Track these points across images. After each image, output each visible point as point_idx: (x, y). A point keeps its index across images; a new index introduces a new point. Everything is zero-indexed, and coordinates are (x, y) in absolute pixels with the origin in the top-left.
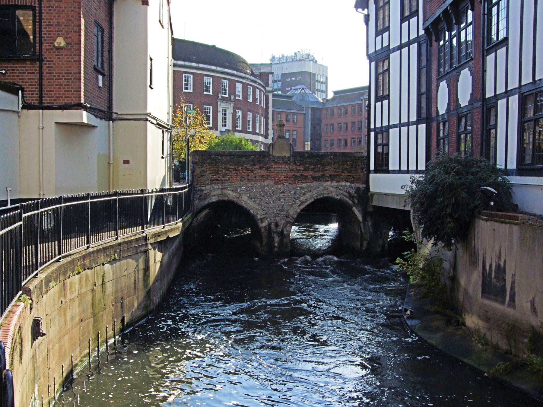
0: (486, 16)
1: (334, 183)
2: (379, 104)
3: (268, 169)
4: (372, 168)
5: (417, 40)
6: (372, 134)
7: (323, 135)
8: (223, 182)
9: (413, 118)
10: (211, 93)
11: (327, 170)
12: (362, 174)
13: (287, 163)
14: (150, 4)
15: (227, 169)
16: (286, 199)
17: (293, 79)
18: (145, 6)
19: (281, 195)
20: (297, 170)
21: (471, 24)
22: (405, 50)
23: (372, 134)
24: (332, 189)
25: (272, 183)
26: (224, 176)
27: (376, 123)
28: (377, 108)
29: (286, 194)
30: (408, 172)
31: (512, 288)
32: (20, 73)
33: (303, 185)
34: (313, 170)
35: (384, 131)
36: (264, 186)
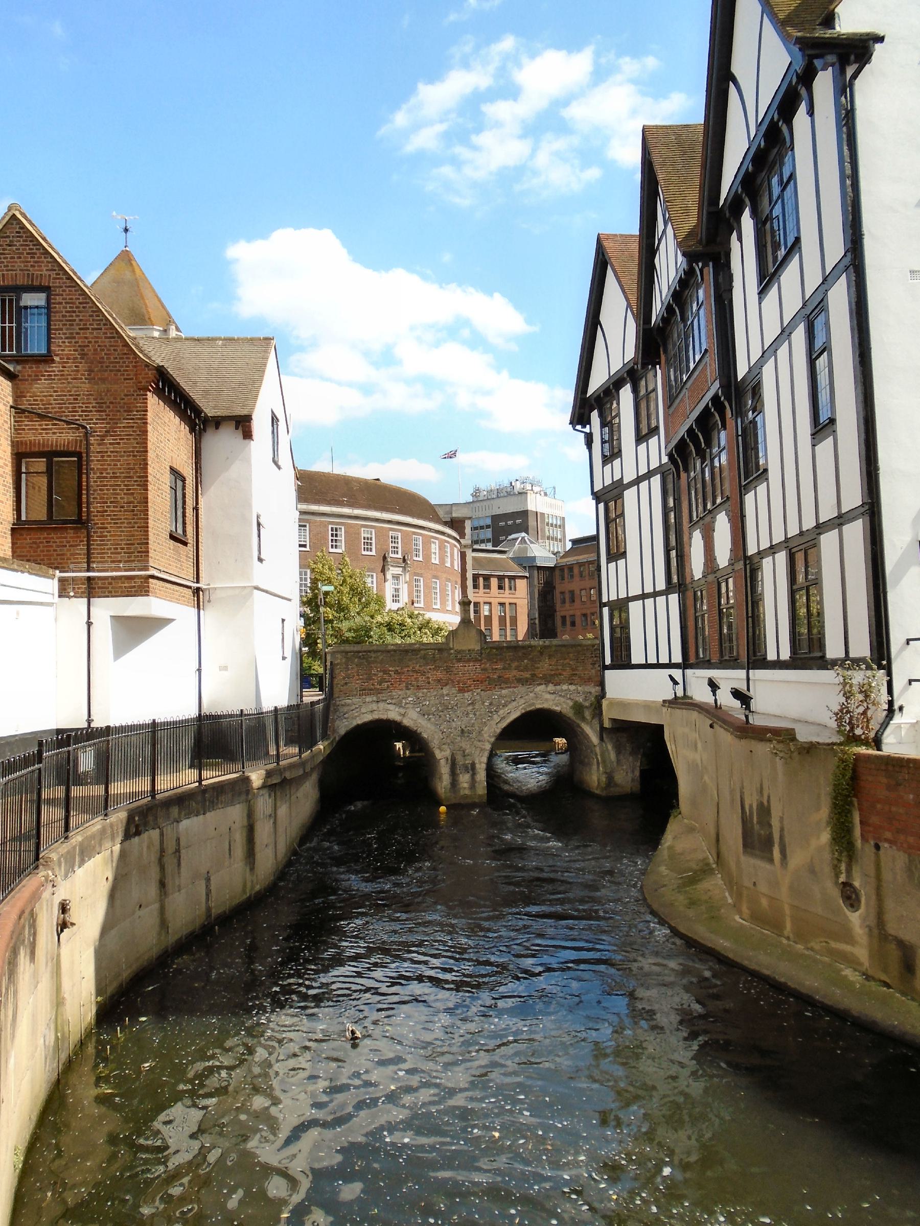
0: (740, 438)
1: (551, 687)
2: (612, 565)
3: (448, 670)
4: (608, 661)
5: (661, 470)
6: (606, 610)
7: (558, 606)
8: (379, 691)
9: (661, 585)
10: (373, 553)
11: (538, 668)
12: (593, 671)
13: (476, 660)
14: (254, 437)
15: (385, 672)
16: (478, 713)
17: (510, 523)
18: (247, 441)
19: (470, 708)
20: (493, 669)
21: (724, 448)
22: (644, 485)
23: (606, 610)
24: (548, 696)
25: (454, 690)
26: (380, 683)
27: (610, 594)
28: (608, 571)
29: (477, 707)
30: (670, 666)
31: (782, 837)
32: (58, 546)
33: (503, 691)
34: (517, 668)
35: (620, 606)
36: (443, 695)
